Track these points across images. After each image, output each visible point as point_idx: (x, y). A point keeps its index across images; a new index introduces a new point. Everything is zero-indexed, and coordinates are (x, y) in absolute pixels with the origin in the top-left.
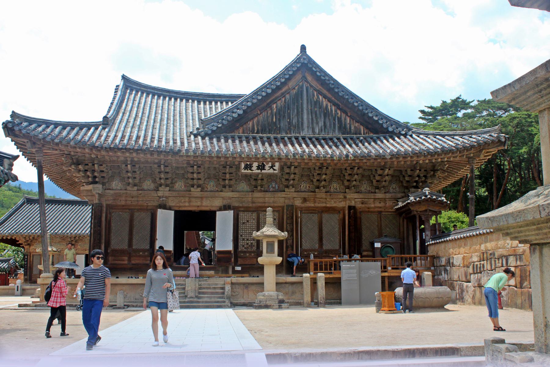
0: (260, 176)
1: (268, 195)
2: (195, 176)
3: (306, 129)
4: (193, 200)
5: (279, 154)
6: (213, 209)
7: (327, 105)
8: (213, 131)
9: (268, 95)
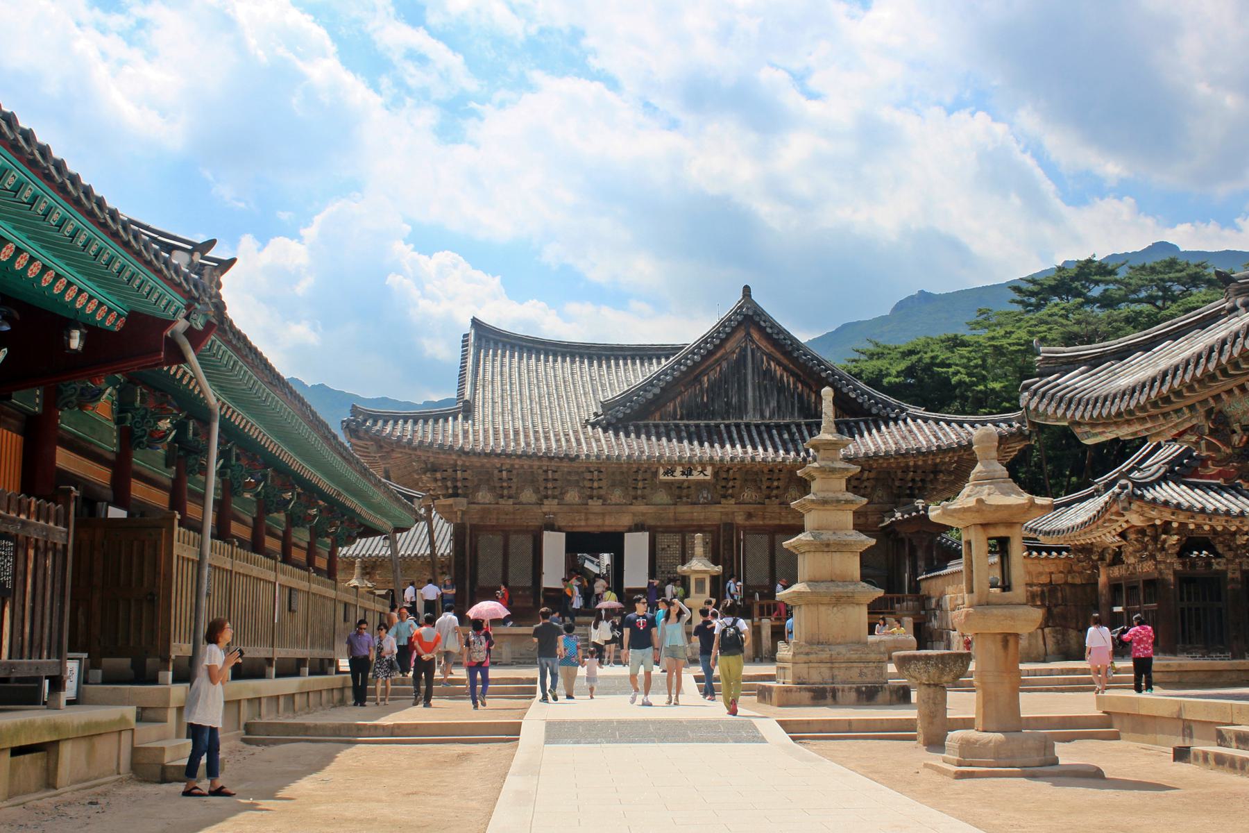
0: (686, 484)
1: (698, 508)
2: (596, 485)
3: (751, 412)
4: (591, 517)
5: (711, 458)
6: (620, 529)
7: (782, 376)
8: (619, 420)
9: (696, 364)
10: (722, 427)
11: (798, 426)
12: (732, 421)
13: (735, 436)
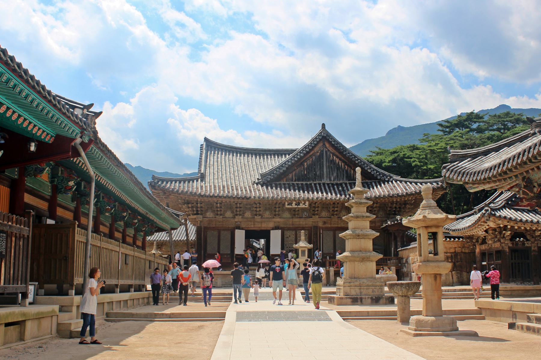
0: (297, 209)
1: (302, 220)
2: (258, 209)
3: (325, 178)
4: (256, 223)
5: (308, 198)
6: (269, 229)
7: (339, 162)
8: (268, 181)
9: (301, 157)
10: (313, 184)
11: (346, 184)
12: (317, 182)
13: (318, 188)
